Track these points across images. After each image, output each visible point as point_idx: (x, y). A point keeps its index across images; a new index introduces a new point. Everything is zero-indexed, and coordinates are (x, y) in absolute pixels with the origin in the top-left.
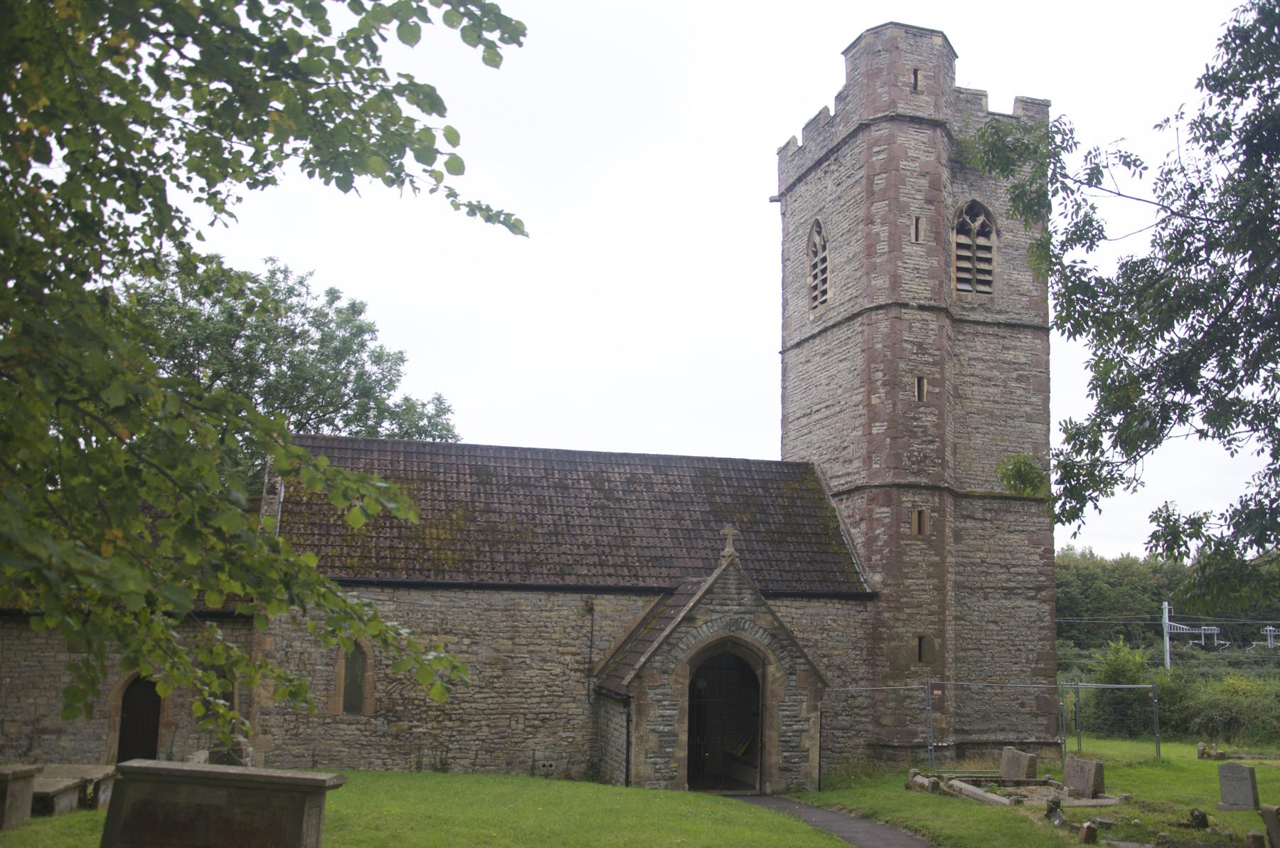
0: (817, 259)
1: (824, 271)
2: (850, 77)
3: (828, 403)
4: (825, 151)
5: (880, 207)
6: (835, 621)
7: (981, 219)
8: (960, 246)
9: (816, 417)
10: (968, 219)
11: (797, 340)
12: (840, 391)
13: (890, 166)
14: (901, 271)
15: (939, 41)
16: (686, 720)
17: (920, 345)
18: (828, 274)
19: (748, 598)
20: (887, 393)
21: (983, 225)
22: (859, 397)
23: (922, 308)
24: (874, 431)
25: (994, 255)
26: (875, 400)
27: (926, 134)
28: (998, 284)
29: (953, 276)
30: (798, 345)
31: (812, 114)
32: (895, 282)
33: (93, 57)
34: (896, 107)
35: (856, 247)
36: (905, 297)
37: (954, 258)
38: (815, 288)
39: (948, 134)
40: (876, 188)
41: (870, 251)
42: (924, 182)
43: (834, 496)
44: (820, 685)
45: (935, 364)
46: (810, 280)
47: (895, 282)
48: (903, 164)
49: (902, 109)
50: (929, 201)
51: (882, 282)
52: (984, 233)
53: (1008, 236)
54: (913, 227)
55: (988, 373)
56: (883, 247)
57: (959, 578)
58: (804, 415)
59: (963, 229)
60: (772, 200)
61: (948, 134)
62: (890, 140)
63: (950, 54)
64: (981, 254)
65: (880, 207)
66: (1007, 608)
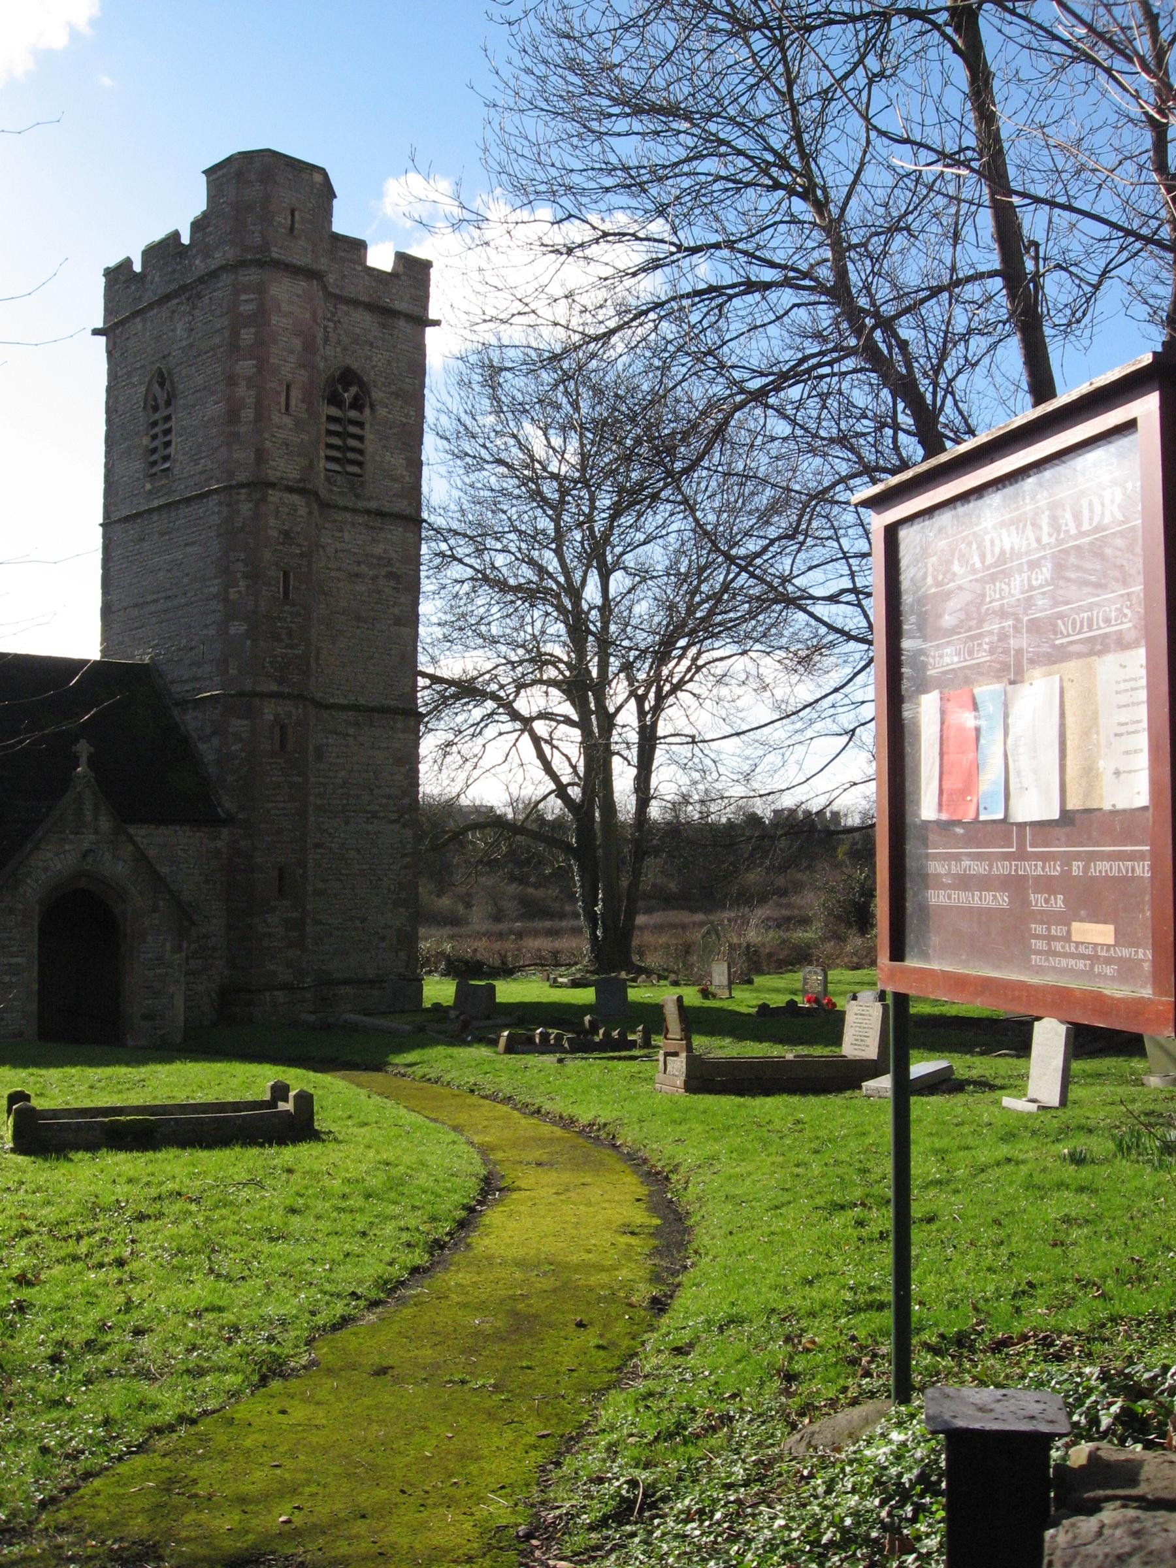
0: (157, 416)
1: (168, 432)
2: (211, 198)
3: (169, 593)
4: (174, 286)
5: (246, 367)
6: (185, 851)
7: (354, 390)
8: (331, 419)
9: (153, 608)
10: (340, 387)
11: (125, 513)
12: (186, 580)
13: (260, 317)
14: (268, 444)
15: (318, 178)
16: (36, 968)
17: (286, 534)
18: (172, 437)
19: (105, 824)
20: (248, 587)
21: (356, 398)
22: (214, 590)
23: (290, 490)
24: (232, 631)
25: (370, 436)
26: (233, 594)
27: (302, 285)
28: (369, 467)
29: (322, 454)
30: (126, 519)
31: (158, 235)
32: (261, 456)
33: (1152, 845)
34: (269, 250)
35: (214, 408)
36: (272, 475)
37: (323, 432)
38: (154, 451)
39: (325, 288)
40: (242, 344)
41: (233, 416)
42: (297, 343)
43: (177, 704)
44: (186, 924)
45: (302, 555)
46: (146, 441)
47: (261, 456)
48: (274, 320)
49: (275, 253)
50: (302, 366)
51: (244, 455)
52: (357, 405)
53: (382, 412)
54: (284, 395)
55: (356, 569)
56: (248, 414)
57: (319, 802)
58: (136, 605)
59: (334, 400)
60: (96, 332)
61: (325, 288)
62: (261, 289)
63: (329, 193)
64: (352, 429)
65: (246, 367)
66: (368, 833)
